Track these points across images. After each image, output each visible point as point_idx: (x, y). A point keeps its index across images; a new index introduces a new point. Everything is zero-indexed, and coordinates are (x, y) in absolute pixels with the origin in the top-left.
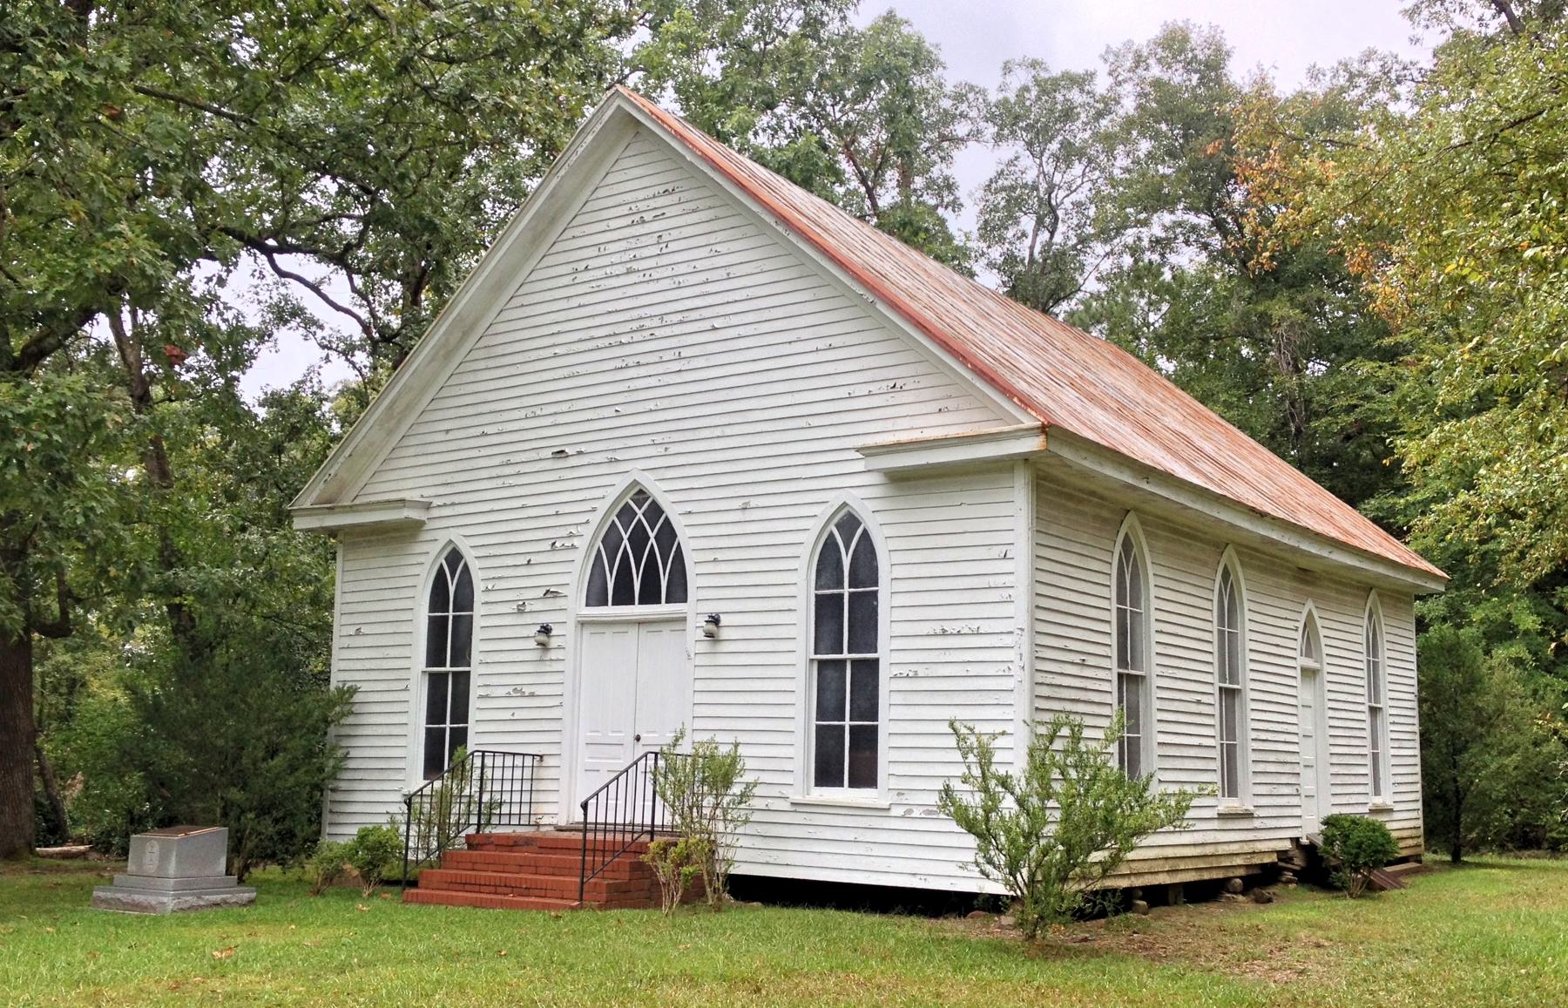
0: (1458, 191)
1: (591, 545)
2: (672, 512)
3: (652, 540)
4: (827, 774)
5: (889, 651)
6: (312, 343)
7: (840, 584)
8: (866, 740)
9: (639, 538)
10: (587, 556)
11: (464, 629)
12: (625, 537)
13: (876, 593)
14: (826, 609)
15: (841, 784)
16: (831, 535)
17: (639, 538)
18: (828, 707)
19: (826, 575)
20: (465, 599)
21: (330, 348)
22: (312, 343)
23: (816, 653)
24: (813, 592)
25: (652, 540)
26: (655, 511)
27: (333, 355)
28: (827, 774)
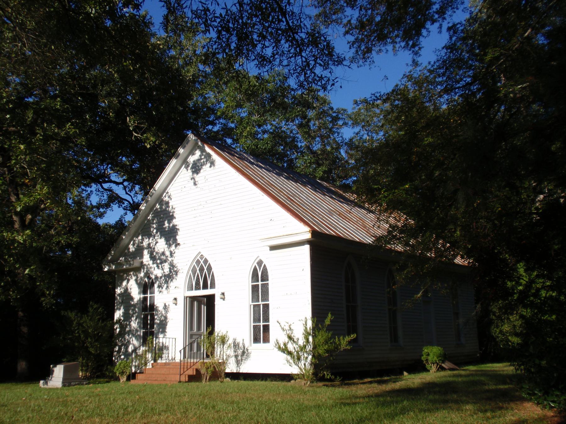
0: (99, 212)
1: (188, 272)
2: (210, 261)
3: (205, 270)
4: (256, 340)
5: (272, 302)
6: (121, 208)
7: (258, 281)
8: (266, 328)
9: (202, 270)
10: (187, 275)
11: (265, 288)
12: (198, 269)
13: (268, 284)
14: (255, 289)
15: (260, 342)
16: (255, 266)
17: (202, 270)
18: (256, 319)
19: (254, 278)
20: (265, 277)
21: (127, 210)
22: (121, 208)
23: (252, 302)
24: (251, 284)
25: (205, 270)
26: (206, 261)
27: (128, 212)
28: (256, 340)
